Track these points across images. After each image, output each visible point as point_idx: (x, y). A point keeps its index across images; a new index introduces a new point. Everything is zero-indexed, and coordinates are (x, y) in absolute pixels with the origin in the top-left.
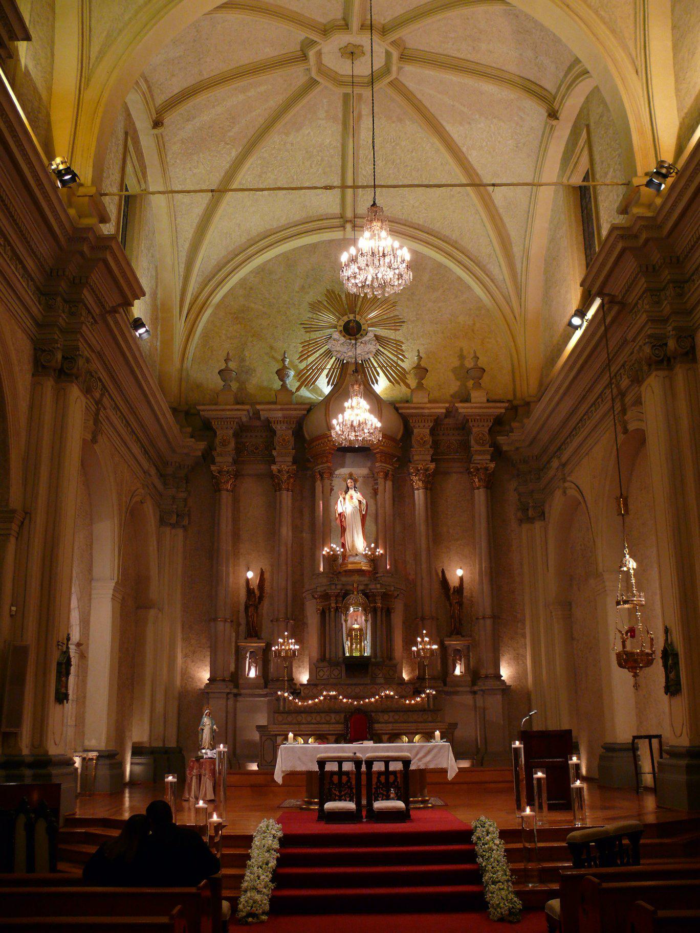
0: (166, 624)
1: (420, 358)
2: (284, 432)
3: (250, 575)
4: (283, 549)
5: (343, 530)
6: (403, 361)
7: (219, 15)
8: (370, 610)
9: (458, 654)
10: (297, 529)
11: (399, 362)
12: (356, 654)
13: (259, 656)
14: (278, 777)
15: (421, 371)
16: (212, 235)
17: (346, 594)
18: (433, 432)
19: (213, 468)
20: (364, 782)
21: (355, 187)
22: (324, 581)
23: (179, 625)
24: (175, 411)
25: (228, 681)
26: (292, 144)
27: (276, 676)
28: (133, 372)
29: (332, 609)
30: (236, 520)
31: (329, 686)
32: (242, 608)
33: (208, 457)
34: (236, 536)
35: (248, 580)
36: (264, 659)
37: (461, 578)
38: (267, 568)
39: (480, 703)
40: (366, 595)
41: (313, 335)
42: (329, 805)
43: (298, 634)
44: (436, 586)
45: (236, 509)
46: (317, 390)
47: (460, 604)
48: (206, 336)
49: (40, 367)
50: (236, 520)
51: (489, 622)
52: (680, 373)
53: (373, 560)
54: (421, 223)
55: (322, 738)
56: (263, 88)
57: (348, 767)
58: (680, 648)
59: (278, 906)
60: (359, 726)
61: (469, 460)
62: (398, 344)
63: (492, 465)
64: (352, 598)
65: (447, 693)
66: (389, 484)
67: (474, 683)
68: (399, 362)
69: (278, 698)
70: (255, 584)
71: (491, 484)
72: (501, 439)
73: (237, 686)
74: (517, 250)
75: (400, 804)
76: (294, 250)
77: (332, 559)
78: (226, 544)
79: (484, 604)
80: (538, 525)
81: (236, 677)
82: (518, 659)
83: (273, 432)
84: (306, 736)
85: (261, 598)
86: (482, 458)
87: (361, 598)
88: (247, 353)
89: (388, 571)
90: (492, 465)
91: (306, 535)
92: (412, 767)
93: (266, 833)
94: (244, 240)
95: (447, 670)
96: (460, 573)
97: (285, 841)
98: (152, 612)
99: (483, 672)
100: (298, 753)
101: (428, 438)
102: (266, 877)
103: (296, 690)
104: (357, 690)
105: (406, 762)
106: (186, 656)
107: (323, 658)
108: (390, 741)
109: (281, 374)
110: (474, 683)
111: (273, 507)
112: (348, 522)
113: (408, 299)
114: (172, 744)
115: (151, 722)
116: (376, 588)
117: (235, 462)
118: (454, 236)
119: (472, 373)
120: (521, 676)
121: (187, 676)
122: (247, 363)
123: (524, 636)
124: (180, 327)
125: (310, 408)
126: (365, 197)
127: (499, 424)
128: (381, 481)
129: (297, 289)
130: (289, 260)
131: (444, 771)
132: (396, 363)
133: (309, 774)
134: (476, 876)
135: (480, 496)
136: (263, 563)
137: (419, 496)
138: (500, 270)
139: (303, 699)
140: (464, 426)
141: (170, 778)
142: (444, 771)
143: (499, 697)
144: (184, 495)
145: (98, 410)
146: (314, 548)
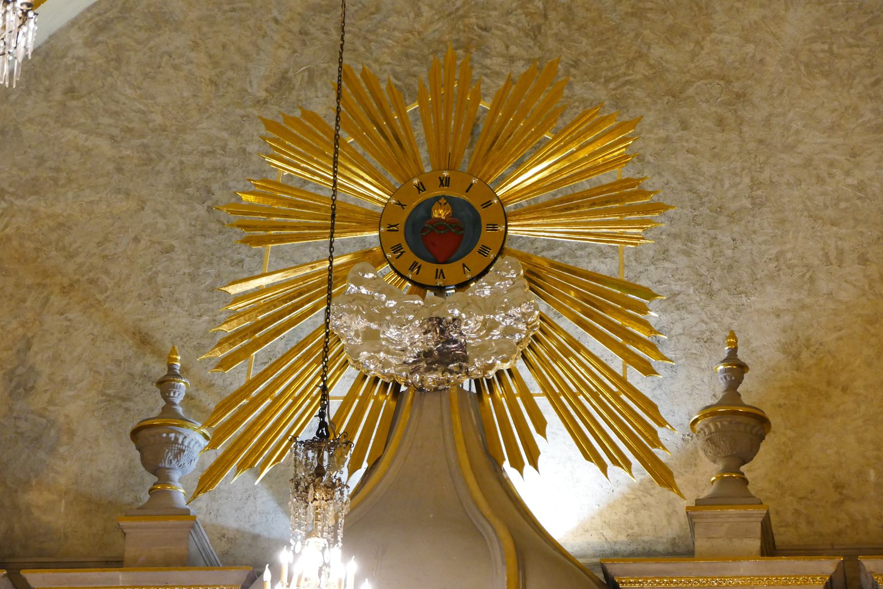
1: (737, 369)
6: (647, 370)
11: (635, 377)
62: (629, 296)
68: (635, 377)
109: (153, 443)
113: (720, 122)
122: (38, 401)
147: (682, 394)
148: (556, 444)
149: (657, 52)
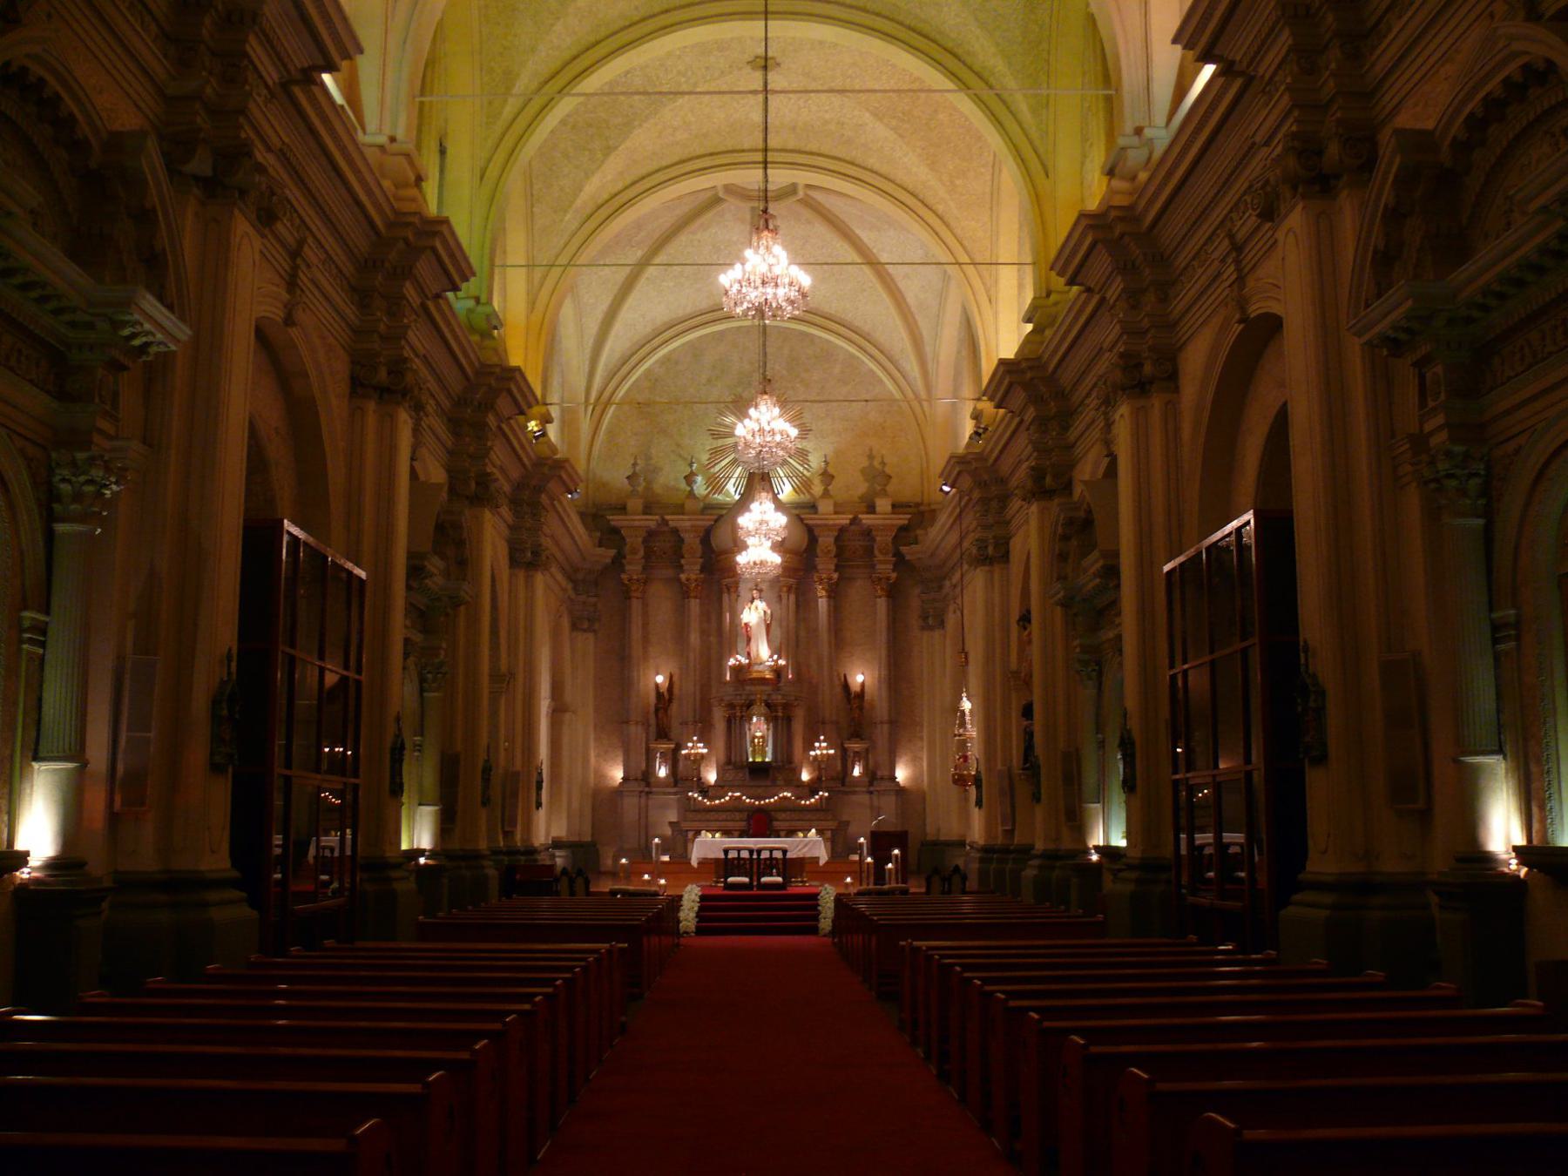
0: (581, 725)
2: (692, 541)
3: (660, 679)
4: (692, 656)
5: (749, 640)
8: (771, 718)
9: (858, 756)
10: (704, 633)
12: (759, 759)
13: (670, 756)
14: (694, 863)
15: (827, 477)
16: (618, 327)
17: (749, 705)
18: (837, 539)
19: (624, 576)
20: (755, 865)
22: (730, 690)
23: (591, 729)
24: (582, 515)
25: (640, 778)
27: (687, 776)
28: (562, 519)
29: (737, 720)
30: (645, 625)
31: (733, 788)
32: (652, 709)
33: (618, 562)
34: (646, 640)
35: (657, 685)
36: (673, 759)
37: (863, 684)
38: (676, 672)
39: (876, 803)
40: (768, 705)
41: (720, 442)
42: (731, 879)
43: (705, 738)
44: (839, 690)
45: (645, 614)
46: (728, 494)
47: (861, 708)
48: (610, 432)
50: (645, 625)
51: (886, 727)
52: (1156, 403)
53: (778, 671)
55: (727, 833)
57: (745, 854)
58: (1136, 735)
59: (700, 931)
60: (760, 823)
61: (873, 566)
63: (894, 575)
64: (755, 708)
65: (846, 793)
66: (792, 597)
67: (871, 784)
69: (689, 798)
70: (664, 689)
71: (894, 593)
72: (904, 549)
73: (648, 785)
74: (928, 349)
75: (780, 879)
77: (738, 669)
78: (636, 649)
79: (882, 710)
80: (937, 634)
81: (647, 776)
82: (915, 760)
83: (682, 540)
84: (713, 831)
85: (670, 700)
86: (885, 568)
87: (763, 709)
88: (653, 451)
89: (789, 681)
90: (894, 575)
91: (713, 639)
92: (789, 855)
93: (691, 895)
94: (649, 330)
95: (847, 771)
96: (860, 678)
97: (703, 898)
98: (567, 716)
99: (879, 774)
100: (709, 845)
101: (833, 549)
102: (693, 915)
103: (705, 790)
104: (759, 791)
105: (785, 852)
106: (598, 756)
107: (729, 762)
108: (787, 836)
109: (689, 479)
110: (871, 784)
111: (681, 610)
112: (753, 633)
114: (588, 839)
115: (569, 817)
116: (778, 698)
117: (644, 568)
118: (866, 328)
119: (879, 477)
120: (916, 778)
121: (601, 776)
123: (921, 738)
124: (585, 425)
125: (721, 506)
127: (904, 534)
128: (784, 596)
130: (695, 350)
131: (817, 859)
133: (717, 860)
134: (816, 918)
135: (882, 604)
136: (672, 666)
137: (823, 604)
138: (912, 367)
139: (711, 799)
140: (868, 533)
141: (624, 861)
142: (817, 859)
143: (894, 798)
144: (593, 600)
146: (721, 660)
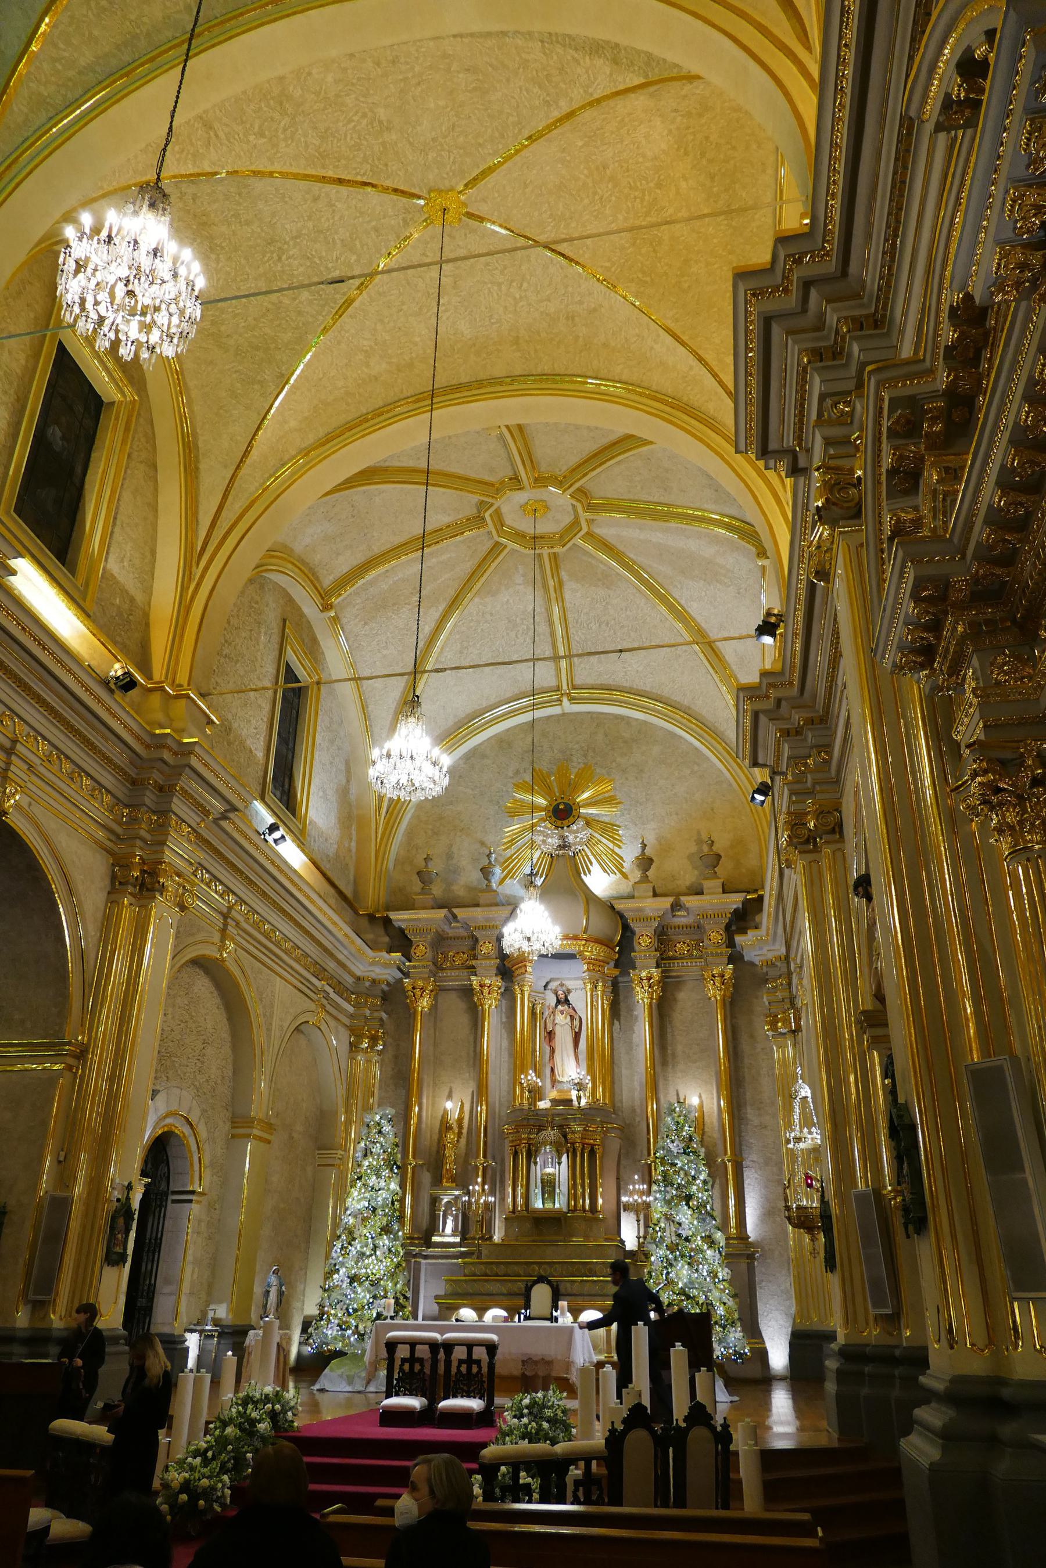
1: (644, 846)
3: (449, 1105)
6: (620, 847)
7: (357, 494)
11: (617, 850)
21: (556, 658)
26: (492, 615)
35: (445, 1111)
49: (117, 884)
54: (648, 689)
56: (445, 557)
68: (617, 850)
76: (508, 730)
122: (454, 861)
126: (582, 665)
129: (511, 774)
132: (613, 851)
145: (225, 925)
147: (629, 853)
148: (595, 868)
149: (618, 759)
